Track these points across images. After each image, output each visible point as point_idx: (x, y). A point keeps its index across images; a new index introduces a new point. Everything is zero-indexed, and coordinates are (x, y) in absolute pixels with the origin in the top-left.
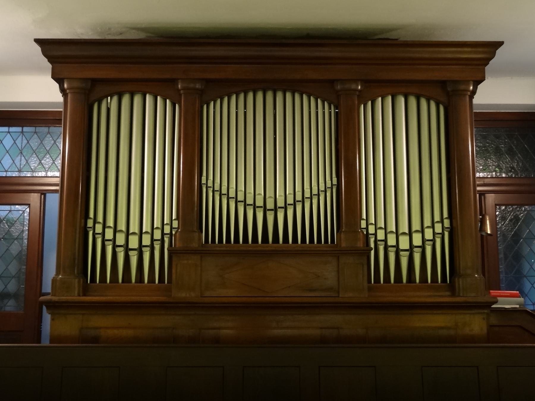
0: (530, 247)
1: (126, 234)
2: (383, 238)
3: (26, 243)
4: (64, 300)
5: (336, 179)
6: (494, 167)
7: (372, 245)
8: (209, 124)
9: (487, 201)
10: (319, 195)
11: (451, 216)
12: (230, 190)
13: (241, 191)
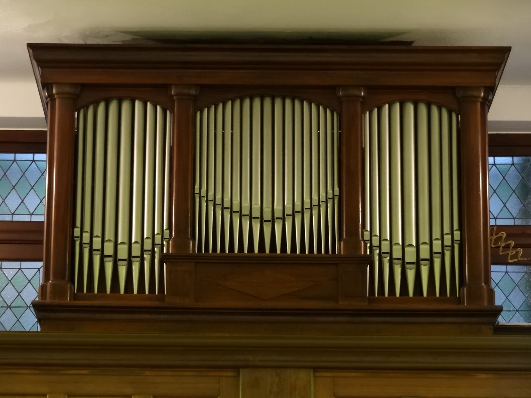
1: (114, 243)
5: (338, 189)
8: (202, 213)
10: (319, 206)
11: (461, 228)
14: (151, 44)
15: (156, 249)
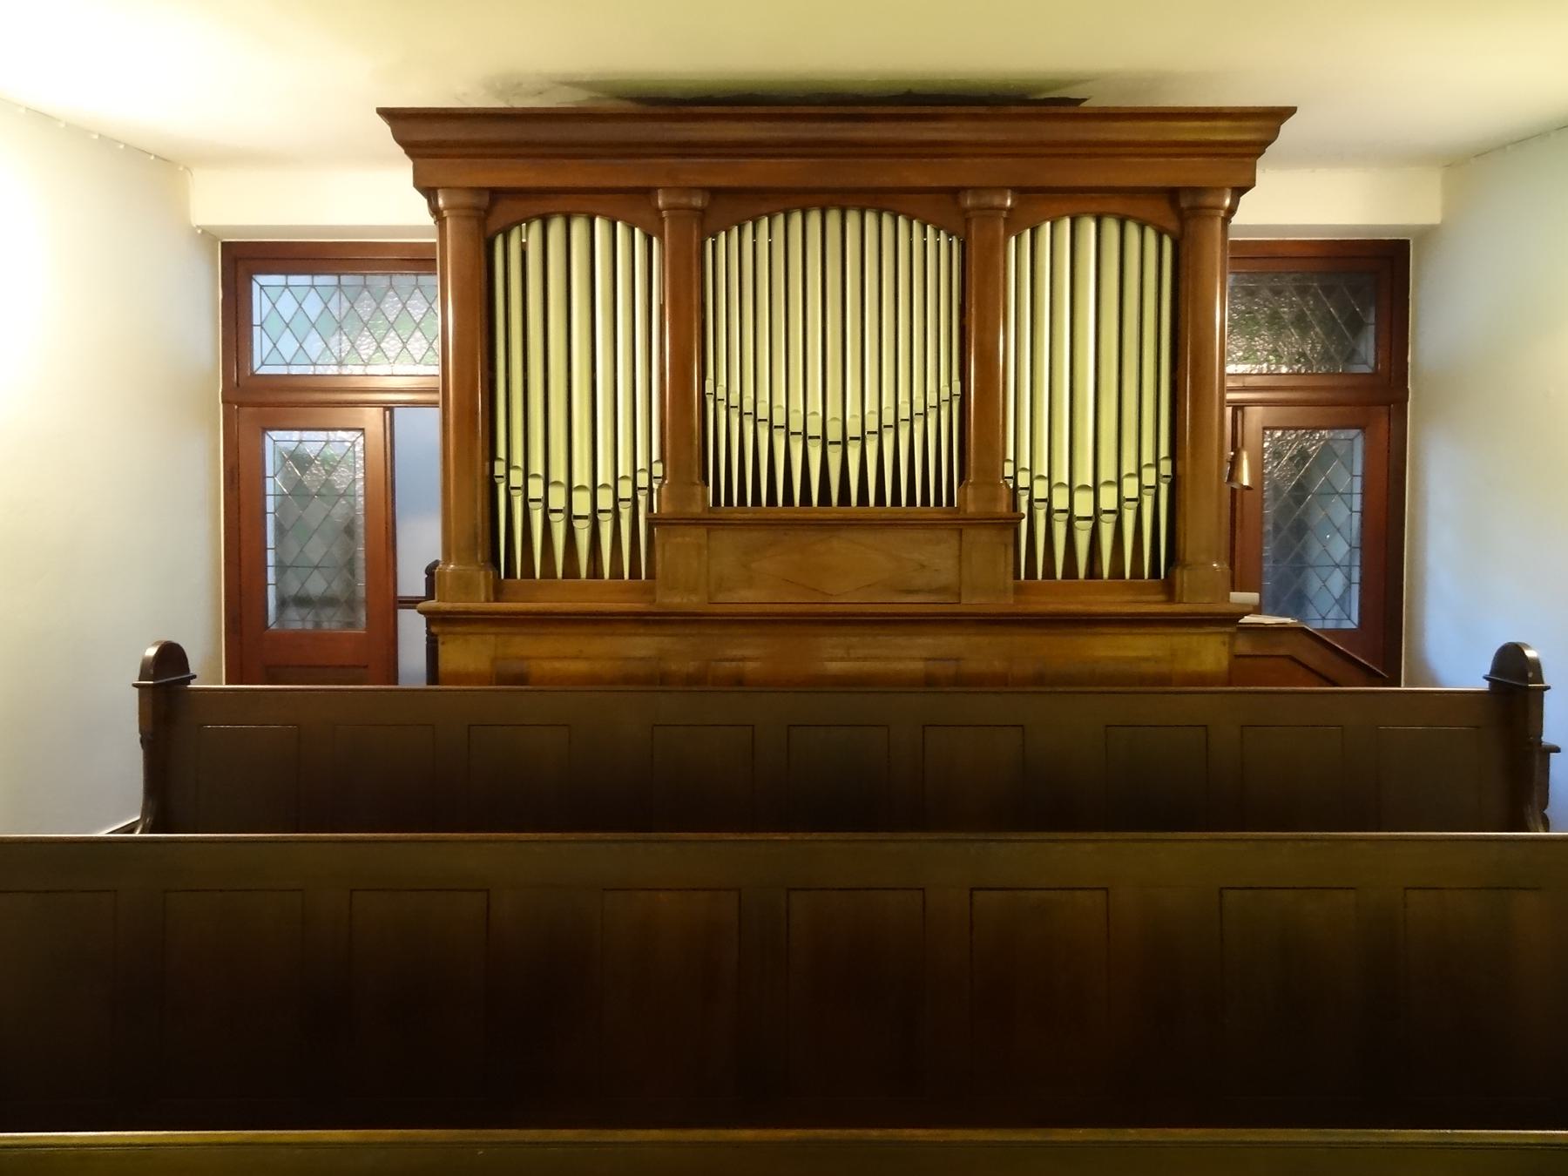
0: (1323, 510)
2: (1045, 496)
3: (362, 503)
4: (461, 609)
5: (959, 383)
6: (1266, 353)
7: (1024, 509)
9: (1246, 419)
11: (1173, 455)
12: (759, 405)
13: (780, 407)
14: (610, 105)
15: (640, 497)
